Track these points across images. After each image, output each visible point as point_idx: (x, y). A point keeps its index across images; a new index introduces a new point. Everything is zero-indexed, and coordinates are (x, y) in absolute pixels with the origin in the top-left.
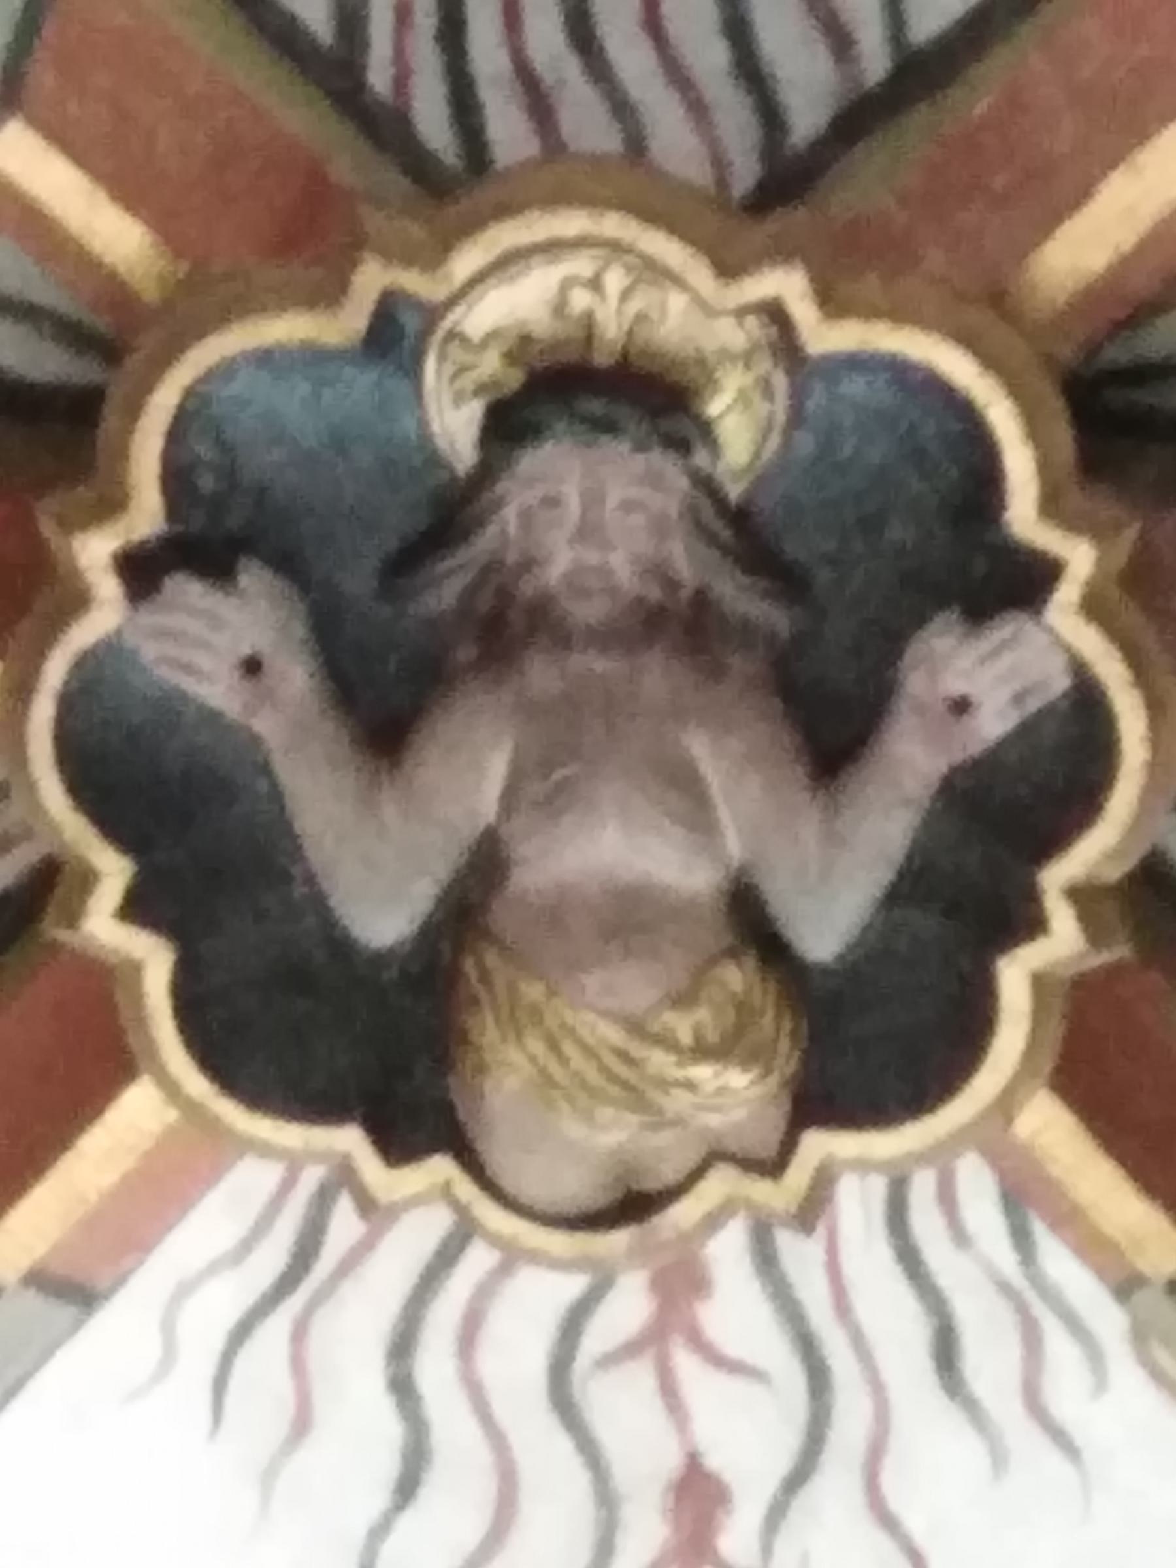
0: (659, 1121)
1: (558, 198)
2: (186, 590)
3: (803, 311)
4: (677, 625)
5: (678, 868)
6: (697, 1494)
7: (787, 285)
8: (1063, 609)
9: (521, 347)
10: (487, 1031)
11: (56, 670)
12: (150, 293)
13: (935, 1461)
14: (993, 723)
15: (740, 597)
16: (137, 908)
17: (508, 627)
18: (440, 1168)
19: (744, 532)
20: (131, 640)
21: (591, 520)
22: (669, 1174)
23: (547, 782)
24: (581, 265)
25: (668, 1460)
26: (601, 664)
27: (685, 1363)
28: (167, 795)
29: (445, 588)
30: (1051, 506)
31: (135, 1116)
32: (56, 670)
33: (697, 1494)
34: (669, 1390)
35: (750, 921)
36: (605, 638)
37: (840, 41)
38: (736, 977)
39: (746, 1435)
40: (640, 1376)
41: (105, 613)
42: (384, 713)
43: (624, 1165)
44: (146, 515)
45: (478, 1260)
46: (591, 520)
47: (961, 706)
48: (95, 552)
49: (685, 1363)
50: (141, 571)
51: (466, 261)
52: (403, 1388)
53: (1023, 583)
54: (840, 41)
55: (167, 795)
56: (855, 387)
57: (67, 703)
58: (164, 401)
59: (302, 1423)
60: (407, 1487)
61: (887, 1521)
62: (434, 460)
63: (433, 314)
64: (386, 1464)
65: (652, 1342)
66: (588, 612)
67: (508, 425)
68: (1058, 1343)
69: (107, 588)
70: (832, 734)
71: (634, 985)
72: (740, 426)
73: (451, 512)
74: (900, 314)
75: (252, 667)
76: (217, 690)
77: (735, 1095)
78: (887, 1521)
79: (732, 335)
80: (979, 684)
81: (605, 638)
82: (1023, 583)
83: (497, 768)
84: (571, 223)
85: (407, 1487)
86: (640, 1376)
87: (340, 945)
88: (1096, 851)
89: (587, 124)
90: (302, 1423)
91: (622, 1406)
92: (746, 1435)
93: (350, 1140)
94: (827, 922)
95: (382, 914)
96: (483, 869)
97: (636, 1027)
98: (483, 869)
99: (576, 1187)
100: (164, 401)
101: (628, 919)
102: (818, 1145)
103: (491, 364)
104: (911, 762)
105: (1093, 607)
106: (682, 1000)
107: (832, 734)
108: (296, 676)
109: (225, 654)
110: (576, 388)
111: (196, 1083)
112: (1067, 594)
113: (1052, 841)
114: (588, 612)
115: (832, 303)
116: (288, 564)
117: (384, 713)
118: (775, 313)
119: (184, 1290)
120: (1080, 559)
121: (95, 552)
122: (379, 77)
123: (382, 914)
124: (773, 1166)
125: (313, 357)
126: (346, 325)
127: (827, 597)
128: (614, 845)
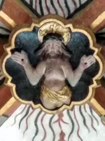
0: (59, 101)
4: (60, 56)
5: (61, 78)
6: (62, 134)
7: (70, 26)
9: (47, 31)
10: (43, 93)
11: (5, 60)
14: (89, 65)
15: (66, 54)
16: (12, 82)
17: (45, 56)
18: (39, 105)
20: (12, 58)
21: (53, 47)
23: (49, 70)
24: (52, 24)
25: (60, 131)
27: (61, 123)
28: (15, 72)
29: (40, 53)
30: (94, 46)
31: (12, 100)
32: (5, 60)
33: (62, 134)
36: (54, 57)
40: (57, 124)
41: (10, 55)
42: (34, 64)
43: (56, 105)
44: (13, 46)
45: (43, 113)
46: (53, 47)
47: (86, 64)
48: (8, 50)
49: (61, 123)
50: (13, 51)
51: (42, 23)
52: (36, 125)
53: (91, 52)
56: (76, 35)
57: (6, 63)
59: (27, 128)
60: (36, 134)
61: (79, 137)
62: (39, 41)
63: (39, 28)
66: (52, 55)
67: (45, 38)
68: (95, 121)
69: (10, 53)
70: (74, 66)
71: (57, 89)
72: (66, 38)
75: (23, 60)
76: (19, 62)
77: (66, 99)
78: (79, 137)
80: (87, 61)
81: (54, 57)
82: (91, 52)
84: (51, 20)
85: (36, 134)
86: (57, 124)
87: (30, 85)
89: (52, 11)
90: (27, 128)
91: (56, 127)
92: (67, 129)
93: (31, 102)
94: (74, 83)
95: (34, 82)
99: (51, 106)
101: (56, 83)
103: (44, 33)
105: (98, 55)
107: (74, 66)
108: (26, 61)
110: (51, 35)
112: (95, 53)
113: (94, 76)
114: (52, 55)
115: (74, 27)
116: (26, 51)
117: (34, 64)
118: (69, 28)
119: (17, 116)
121: (8, 50)
122: (34, 7)
124: (69, 105)
126: (31, 29)
127: (74, 54)
128: (55, 76)
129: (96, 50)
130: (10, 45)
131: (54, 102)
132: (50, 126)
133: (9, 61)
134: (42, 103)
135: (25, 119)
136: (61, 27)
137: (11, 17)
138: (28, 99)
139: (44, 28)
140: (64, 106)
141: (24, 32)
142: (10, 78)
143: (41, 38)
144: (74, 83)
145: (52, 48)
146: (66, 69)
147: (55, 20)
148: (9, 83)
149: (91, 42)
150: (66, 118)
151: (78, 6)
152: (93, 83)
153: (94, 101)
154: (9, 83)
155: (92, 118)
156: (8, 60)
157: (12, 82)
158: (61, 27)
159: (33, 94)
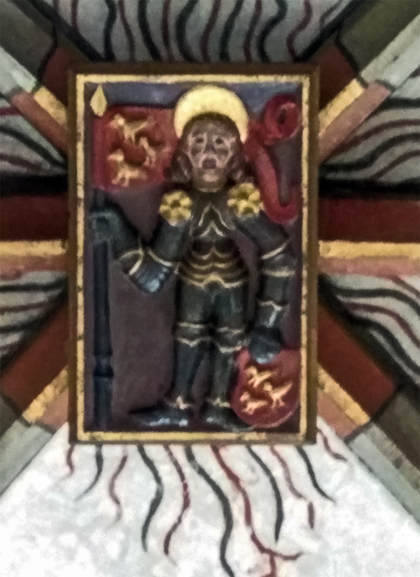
90: (186, 504)
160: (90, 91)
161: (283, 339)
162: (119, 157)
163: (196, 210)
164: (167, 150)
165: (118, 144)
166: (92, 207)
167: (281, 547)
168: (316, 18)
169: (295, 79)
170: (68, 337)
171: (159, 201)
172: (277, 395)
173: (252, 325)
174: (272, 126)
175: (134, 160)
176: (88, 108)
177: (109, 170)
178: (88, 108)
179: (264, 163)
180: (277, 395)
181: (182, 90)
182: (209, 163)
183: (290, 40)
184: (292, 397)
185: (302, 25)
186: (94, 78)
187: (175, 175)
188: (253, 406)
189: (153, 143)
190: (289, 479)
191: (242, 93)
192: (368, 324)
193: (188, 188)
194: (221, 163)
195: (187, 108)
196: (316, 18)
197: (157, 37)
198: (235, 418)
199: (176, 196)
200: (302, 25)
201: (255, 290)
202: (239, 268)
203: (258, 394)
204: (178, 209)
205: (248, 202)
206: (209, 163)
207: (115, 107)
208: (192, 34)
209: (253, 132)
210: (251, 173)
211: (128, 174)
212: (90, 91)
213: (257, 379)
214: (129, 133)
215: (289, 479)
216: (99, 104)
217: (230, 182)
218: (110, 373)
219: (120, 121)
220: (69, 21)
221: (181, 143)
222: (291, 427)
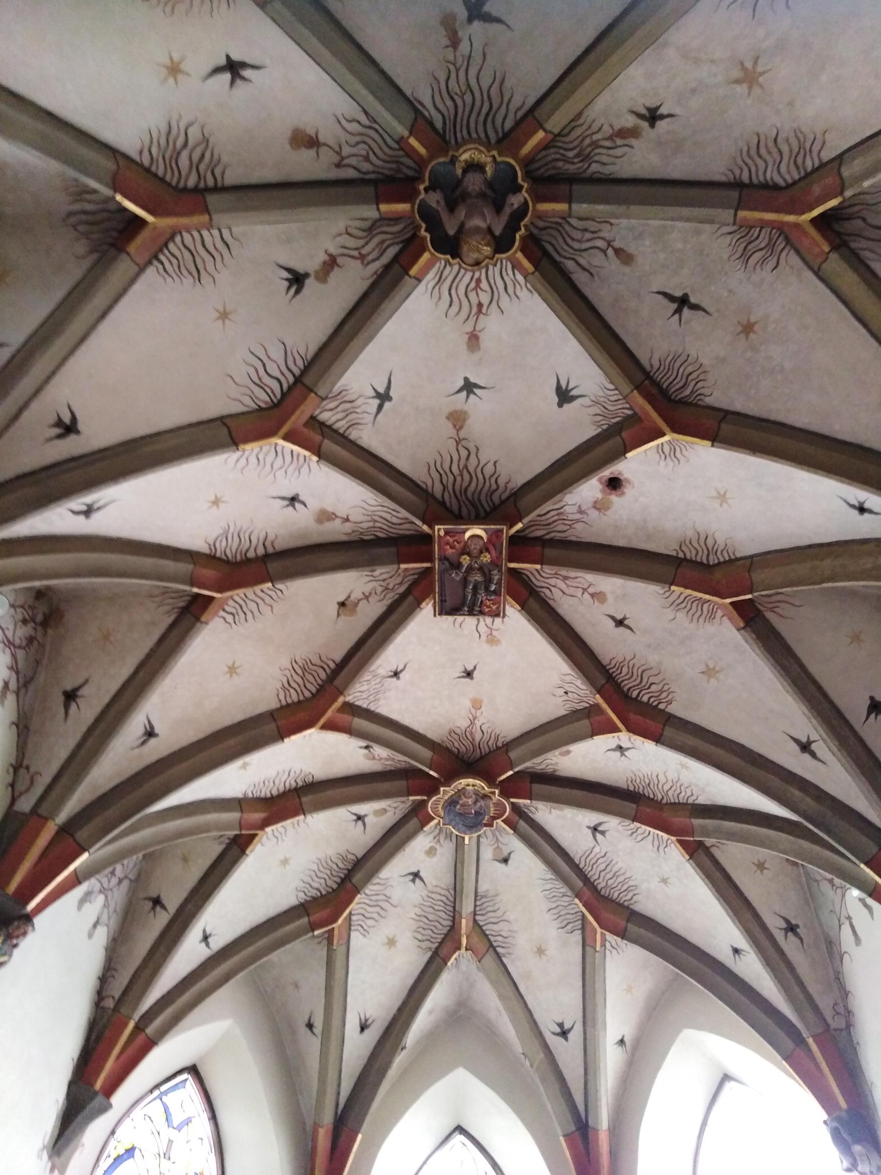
0: (481, 254)
1: (470, 143)
2: (431, 192)
3: (497, 156)
4: (482, 195)
5: (483, 225)
6: (480, 305)
7: (495, 153)
8: (524, 193)
9: (466, 161)
10: (463, 244)
11: (418, 202)
12: (426, 157)
13: (505, 301)
14: (516, 206)
15: (489, 192)
16: (426, 230)
17: (465, 196)
18: (458, 260)
19: (490, 184)
20: (426, 199)
21: (474, 183)
22: (481, 259)
23: (469, 215)
24: (473, 151)
25: (477, 302)
26: (475, 200)
27: (479, 291)
28: (429, 216)
29: (458, 193)
30: (523, 180)
31: (426, 256)
32: (418, 202)
33: (480, 305)
34: (477, 294)
35: (490, 230)
36: (476, 197)
37: (496, 132)
38: (489, 237)
39: (485, 298)
40: (474, 292)
41: (422, 196)
42: (451, 207)
43: (477, 259)
44: (427, 183)
45: (462, 271)
46: (474, 183)
47: (512, 204)
48: (422, 187)
49: (479, 291)
50: (426, 190)
51: (461, 151)
52: (450, 294)
53: (519, 189)
54: (496, 132)
55: (429, 216)
56: (502, 166)
57: (419, 206)
58: (429, 168)
59: (440, 298)
60: (450, 305)
61: (499, 307)
62: (456, 176)
63: (457, 157)
64: (448, 304)
65: (475, 289)
66: (474, 194)
67: (465, 171)
68: (518, 286)
69: (423, 192)
70: (499, 209)
71: (478, 237)
72: (489, 170)
73: (459, 182)
74: (507, 156)
75: (438, 202)
76: (434, 205)
77: (487, 250)
78: (499, 307)
79: (489, 159)
80: (515, 201)
81: (476, 197)
82: (519, 189)
83: (463, 213)
84: (472, 146)
85: (450, 305)
86: (474, 292)
87: (447, 234)
88: (526, 220)
89: (474, 135)
90: (440, 298)
91: (472, 296)
92: (485, 298)
93: (449, 257)
94: (497, 232)
95: (451, 232)
96: (462, 227)
97: (478, 243)
98: (462, 227)
99: (470, 261)
100: (429, 168)
101: (477, 230)
102: (497, 256)
103: (463, 164)
104: (507, 211)
105: (527, 191)
106: (483, 240)
107: (499, 209)
108: (442, 203)
109: (434, 199)
110: (474, 167)
111: (432, 250)
112: (524, 190)
113: (522, 219)
114: (474, 194)
115: (500, 155)
116: (442, 189)
117: (451, 207)
118: (494, 157)
119: (428, 283)
120: (526, 185)
121: (422, 187)
122: (447, 138)
123: (451, 232)
124: (492, 259)
125: (445, 163)
126: (447, 159)
127: (500, 189)
128: (477, 222)
129: (526, 185)
130: (423, 182)
131: (476, 255)
132: (467, 296)
133: (423, 201)
134: (670, 719)
135: (437, 287)
136: (484, 157)
137: (421, 795)
138: (444, 253)
139: (465, 157)
140: (487, 261)
141: (439, 163)
142: (424, 225)
143: (459, 172)
144: (497, 232)
145: (474, 184)
146: (488, 212)
147: (477, 146)
148: (423, 232)
149: (519, 174)
150: (484, 285)
151: (501, 135)
152: (520, 229)
153: (519, 255)
154: (423, 232)
155: (515, 282)
156: (421, 201)
157: (426, 230)
158: (484, 157)
159: (450, 246)
160: (439, 530)
161: (497, 593)
162: (448, 547)
163: (471, 560)
164: (462, 544)
165: (448, 544)
166: (440, 560)
167: (494, 627)
168: (508, 491)
169: (501, 527)
170: (432, 584)
171: (459, 557)
172: (494, 607)
173: (487, 589)
174: (494, 538)
175: (452, 547)
176: (439, 534)
177: (445, 550)
178: (439, 534)
179: (491, 548)
180: (494, 607)
181: (467, 530)
182: (474, 547)
183: (500, 497)
184: (498, 608)
185: (504, 492)
186: (440, 527)
187: (465, 551)
188: (487, 610)
189: (458, 543)
190: (496, 112)
191: (485, 530)
192: (522, 573)
193: (469, 554)
194: (478, 547)
195: (468, 535)
196: (508, 491)
197: (458, 493)
198: (481, 613)
199: (465, 556)
200: (504, 492)
201: (488, 581)
202: (484, 574)
203: (488, 607)
204: (465, 560)
205: (486, 558)
206: (474, 547)
207: (447, 533)
208: (469, 494)
209: (488, 539)
210: (488, 550)
211: (450, 551)
212: (439, 530)
213: (488, 603)
214: (451, 540)
215: (496, 112)
216: (442, 533)
217: (481, 552)
218: (445, 601)
219: (448, 538)
220: (401, 246)
221: (466, 543)
222: (498, 615)
